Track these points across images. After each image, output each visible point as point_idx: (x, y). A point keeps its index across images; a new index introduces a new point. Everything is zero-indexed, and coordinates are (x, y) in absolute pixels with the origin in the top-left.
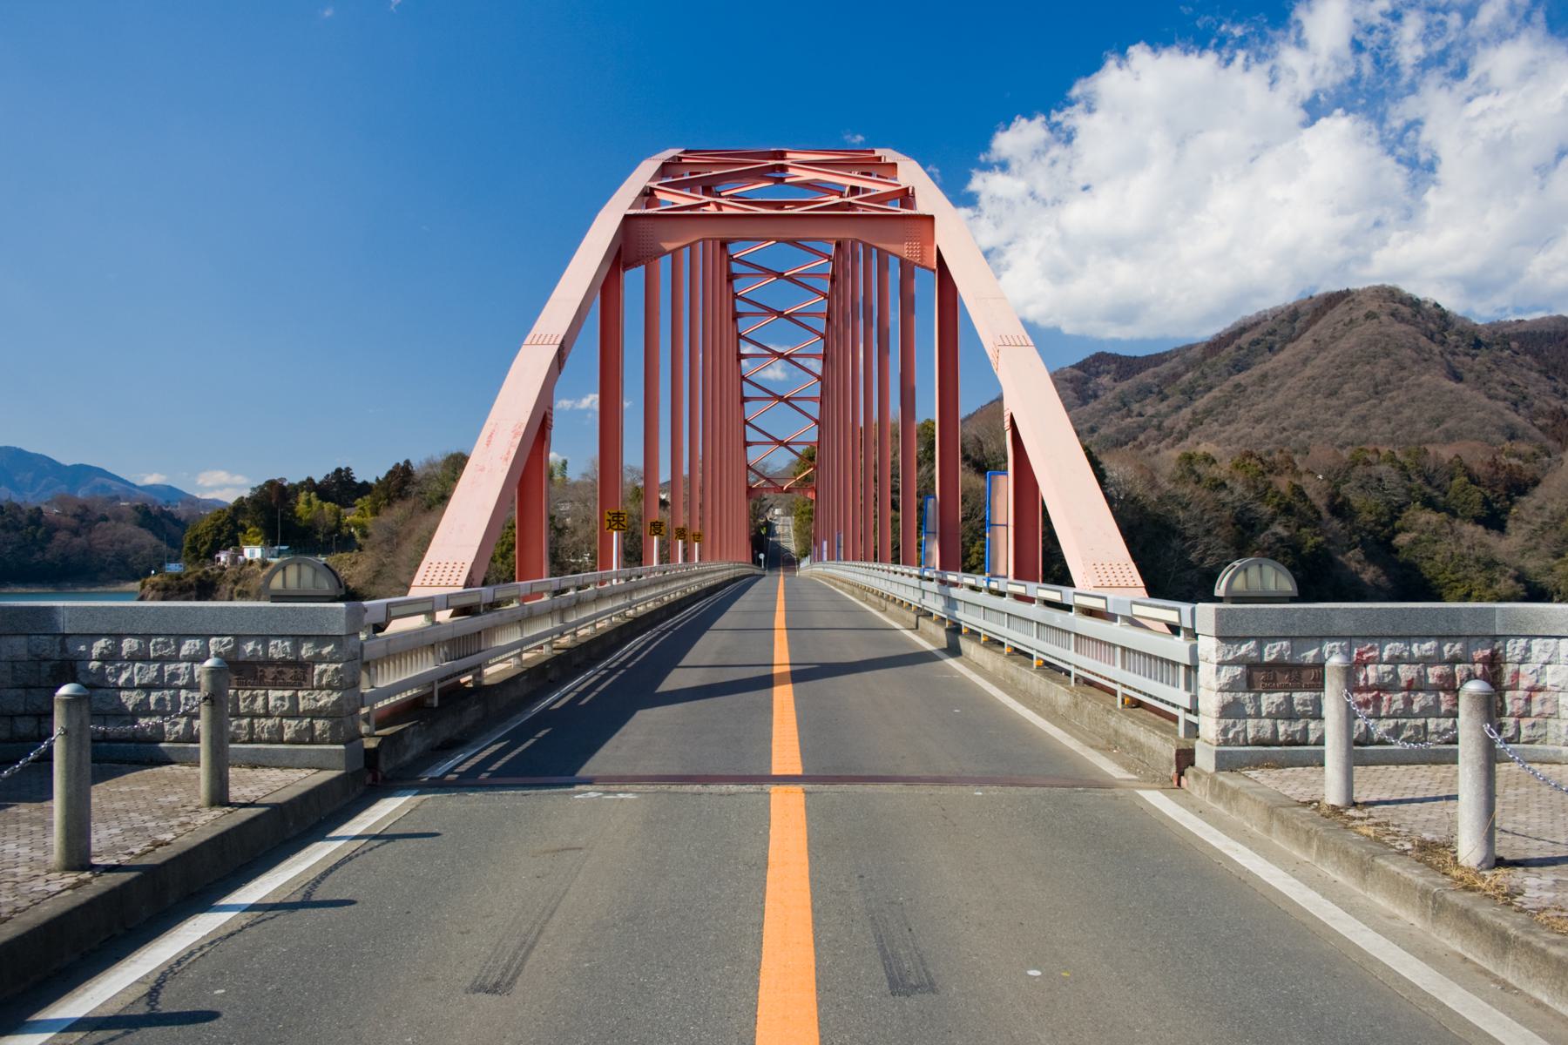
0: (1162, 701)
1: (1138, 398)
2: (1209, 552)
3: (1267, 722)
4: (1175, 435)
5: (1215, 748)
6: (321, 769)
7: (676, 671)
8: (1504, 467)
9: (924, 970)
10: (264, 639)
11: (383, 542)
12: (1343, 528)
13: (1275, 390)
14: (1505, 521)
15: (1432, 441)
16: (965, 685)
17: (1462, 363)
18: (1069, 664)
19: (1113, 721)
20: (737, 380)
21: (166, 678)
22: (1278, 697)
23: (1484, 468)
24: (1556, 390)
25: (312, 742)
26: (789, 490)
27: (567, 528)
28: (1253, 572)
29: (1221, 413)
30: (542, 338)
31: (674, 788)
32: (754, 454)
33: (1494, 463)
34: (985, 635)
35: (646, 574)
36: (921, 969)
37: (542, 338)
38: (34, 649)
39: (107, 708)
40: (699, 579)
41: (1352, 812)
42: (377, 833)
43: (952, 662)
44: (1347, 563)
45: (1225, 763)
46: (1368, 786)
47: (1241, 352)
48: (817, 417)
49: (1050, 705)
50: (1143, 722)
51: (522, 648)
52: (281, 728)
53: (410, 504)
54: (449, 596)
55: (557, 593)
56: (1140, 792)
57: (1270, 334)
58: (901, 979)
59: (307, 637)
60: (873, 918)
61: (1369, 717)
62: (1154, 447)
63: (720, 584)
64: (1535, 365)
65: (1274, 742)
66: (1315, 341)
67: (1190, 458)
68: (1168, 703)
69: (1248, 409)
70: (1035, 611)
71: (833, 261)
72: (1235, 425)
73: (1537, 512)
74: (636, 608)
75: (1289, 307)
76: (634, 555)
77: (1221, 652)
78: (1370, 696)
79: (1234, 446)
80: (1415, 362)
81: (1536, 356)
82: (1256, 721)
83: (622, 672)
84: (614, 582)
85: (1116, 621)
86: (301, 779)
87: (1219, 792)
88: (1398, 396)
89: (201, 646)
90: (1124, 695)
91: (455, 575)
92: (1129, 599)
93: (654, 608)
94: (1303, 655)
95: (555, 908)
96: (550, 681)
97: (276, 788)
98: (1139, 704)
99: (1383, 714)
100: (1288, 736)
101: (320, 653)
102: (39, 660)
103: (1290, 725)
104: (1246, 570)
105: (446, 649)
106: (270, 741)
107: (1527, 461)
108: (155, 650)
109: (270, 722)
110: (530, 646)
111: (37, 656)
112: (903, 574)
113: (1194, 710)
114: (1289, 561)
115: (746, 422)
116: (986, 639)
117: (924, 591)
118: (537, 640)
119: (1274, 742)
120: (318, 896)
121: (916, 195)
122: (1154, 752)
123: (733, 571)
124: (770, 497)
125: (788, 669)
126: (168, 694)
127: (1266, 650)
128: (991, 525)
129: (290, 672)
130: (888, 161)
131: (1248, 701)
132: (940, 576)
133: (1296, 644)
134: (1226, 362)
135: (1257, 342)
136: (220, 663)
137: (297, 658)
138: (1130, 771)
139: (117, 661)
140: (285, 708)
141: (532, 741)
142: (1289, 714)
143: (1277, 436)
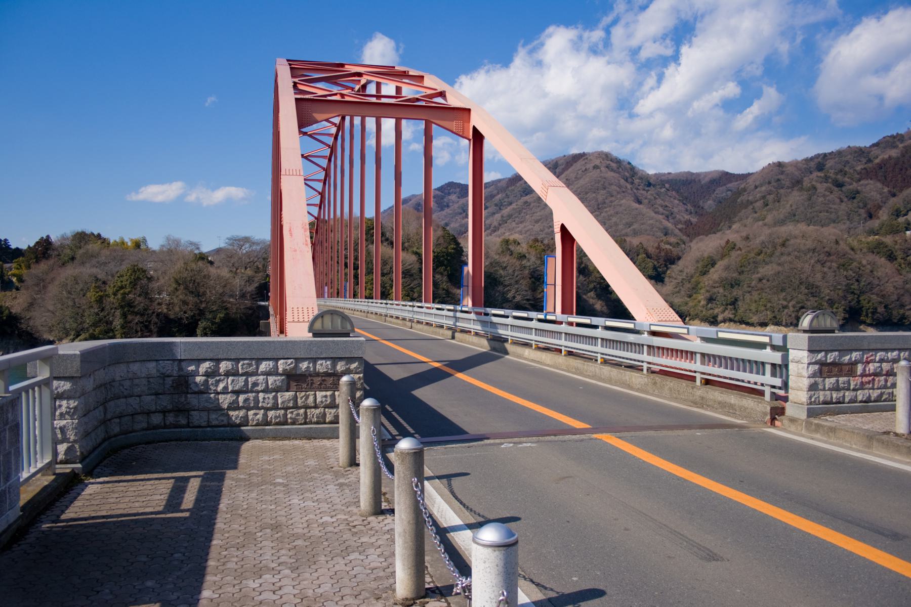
3: (828, 392)
4: (492, 228)
5: (807, 406)
8: (664, 250)
10: (314, 360)
11: (33, 285)
12: (585, 281)
14: (664, 278)
15: (627, 235)
17: (642, 194)
21: (250, 386)
22: (833, 380)
23: (653, 250)
24: (687, 210)
33: (658, 248)
38: (161, 370)
39: (211, 406)
44: (588, 299)
52: (325, 415)
59: (341, 359)
61: (870, 389)
64: (677, 196)
66: (567, 179)
73: (680, 273)
75: (553, 161)
77: (809, 358)
78: (870, 378)
80: (618, 193)
81: (677, 192)
82: (823, 392)
88: (610, 210)
89: (273, 366)
94: (843, 358)
99: (876, 387)
101: (349, 368)
102: (164, 376)
106: (317, 423)
107: (674, 247)
108: (242, 369)
109: (318, 411)
111: (162, 374)
119: (831, 403)
126: (251, 396)
127: (829, 356)
134: (519, 189)
139: (215, 376)
140: (328, 402)
141: (394, 413)
142: (836, 388)
143: (547, 230)
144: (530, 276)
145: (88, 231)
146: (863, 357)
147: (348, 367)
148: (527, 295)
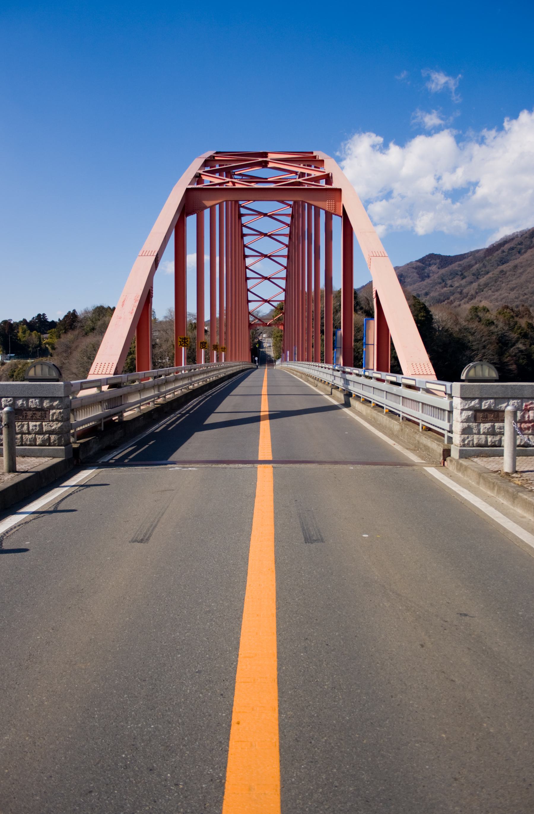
0: (438, 427)
1: (451, 277)
2: (485, 357)
3: (483, 437)
4: (469, 297)
6: (54, 457)
7: (213, 415)
9: (320, 534)
10: (27, 399)
11: (63, 352)
13: (521, 273)
16: (352, 421)
18: (400, 411)
19: (417, 437)
20: (243, 268)
22: (488, 425)
25: (49, 445)
26: (270, 325)
27: (157, 344)
28: (478, 368)
29: (493, 286)
30: (148, 252)
31: (214, 466)
32: (252, 306)
34: (363, 398)
35: (198, 368)
36: (318, 534)
37: (148, 252)
40: (225, 370)
41: (514, 475)
42: (82, 484)
43: (346, 410)
45: (463, 455)
46: (525, 465)
47: (504, 254)
48: (284, 288)
49: (391, 430)
50: (430, 437)
51: (140, 404)
52: (35, 439)
53: (76, 332)
54: (107, 379)
55: (155, 377)
56: (425, 468)
57: (519, 244)
58: (310, 538)
59: (46, 398)
60: (300, 516)
62: (458, 303)
63: (235, 373)
65: (486, 445)
67: (476, 309)
68: (441, 428)
69: (507, 284)
70: (385, 386)
71: (293, 207)
72: (500, 292)
74: (193, 385)
75: (529, 230)
76: (192, 359)
77: (462, 405)
78: (530, 425)
79: (500, 303)
82: (478, 436)
83: (188, 415)
84: (183, 372)
85: (419, 390)
86: (46, 462)
87: (460, 468)
90: (423, 425)
91: (109, 369)
92: (425, 380)
93: (203, 385)
94: (500, 406)
95: (164, 513)
96: (154, 419)
97: (36, 465)
98: (430, 429)
100: (493, 443)
101: (52, 405)
103: (493, 438)
104: (475, 367)
105: (107, 404)
106: (30, 445)
109: (30, 436)
110: (144, 403)
112: (325, 368)
113: (451, 431)
114: (525, 362)
115: (248, 290)
116: (364, 399)
117: (335, 376)
118: (148, 400)
119: (486, 445)
120: (60, 508)
121: (333, 177)
122: (434, 450)
123: (241, 366)
124: (261, 328)
125: (267, 413)
127: (483, 404)
128: (366, 344)
129: (39, 414)
130: (320, 158)
131: (474, 427)
132: (342, 369)
133: (497, 401)
134: (496, 259)
135: (512, 249)
136: (11, 409)
137: (42, 407)
138: (423, 459)
140: (37, 430)
141: (147, 446)
144: (497, 341)
145: (106, 306)
146: (522, 405)
147: (51, 404)
148: (493, 359)
